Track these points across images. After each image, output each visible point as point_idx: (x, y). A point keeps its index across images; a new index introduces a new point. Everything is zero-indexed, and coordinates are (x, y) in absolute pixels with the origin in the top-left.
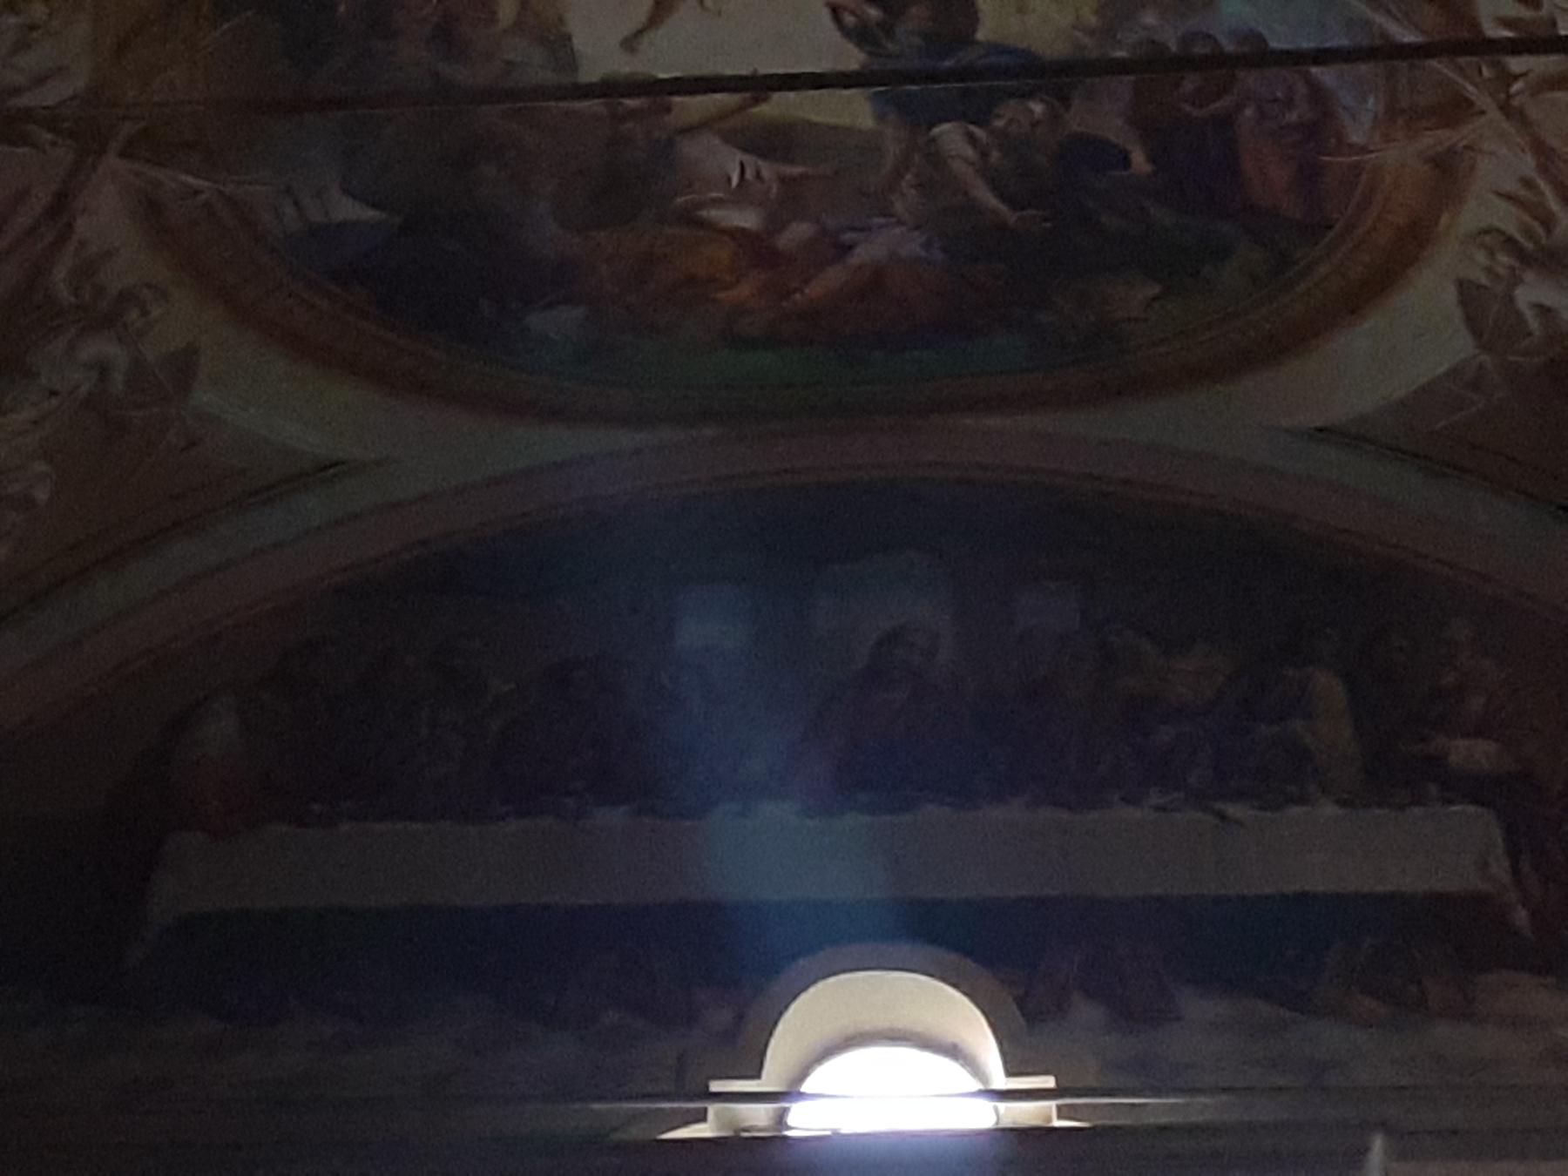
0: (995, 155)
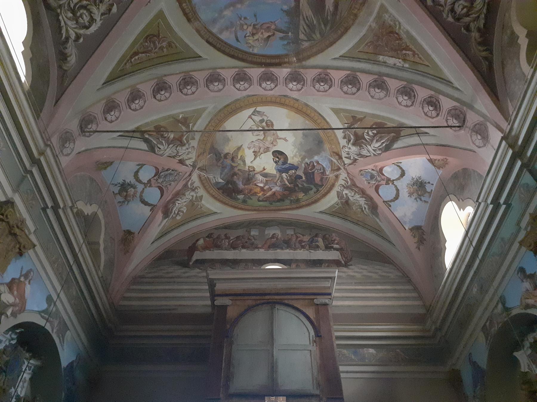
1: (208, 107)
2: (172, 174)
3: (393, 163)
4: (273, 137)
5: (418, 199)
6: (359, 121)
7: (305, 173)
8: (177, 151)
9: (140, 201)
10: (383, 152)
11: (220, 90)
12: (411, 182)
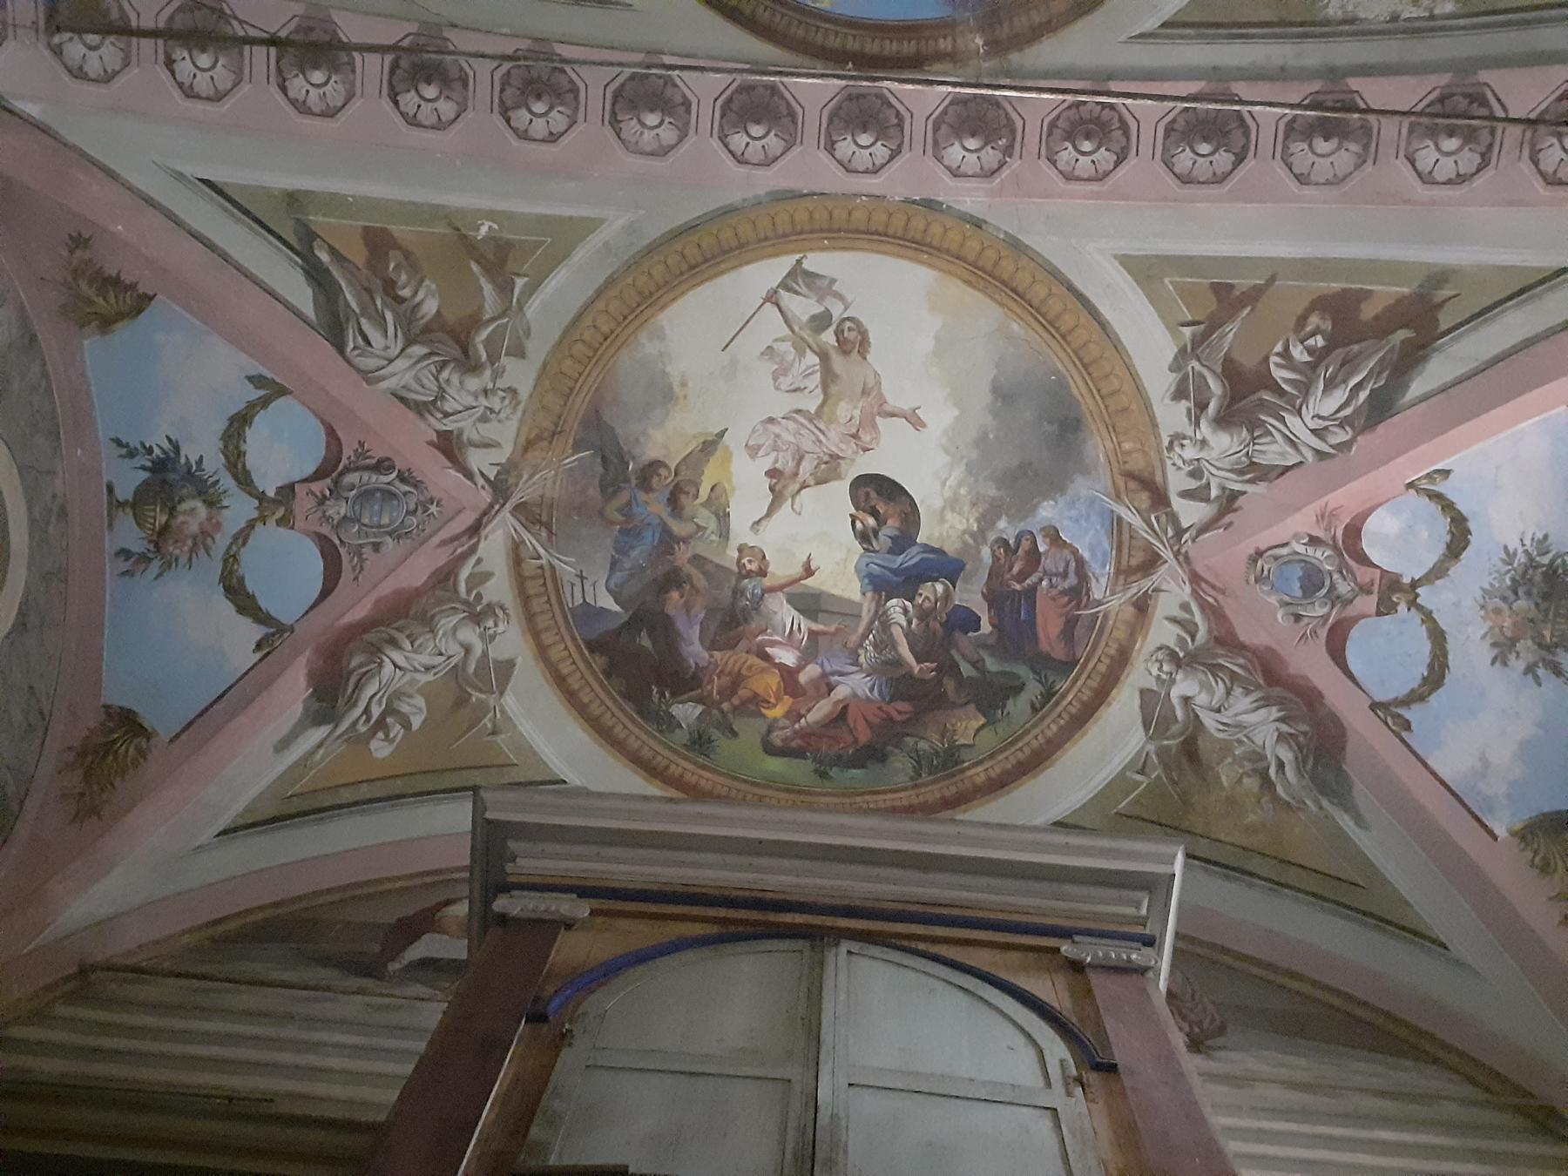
1: (602, 221)
2: (394, 495)
3: (1410, 485)
4: (860, 405)
5: (1541, 672)
6: (1244, 306)
7: (994, 598)
8: (440, 387)
9: (223, 579)
10: (1362, 431)
11: (663, 151)
12: (1502, 575)
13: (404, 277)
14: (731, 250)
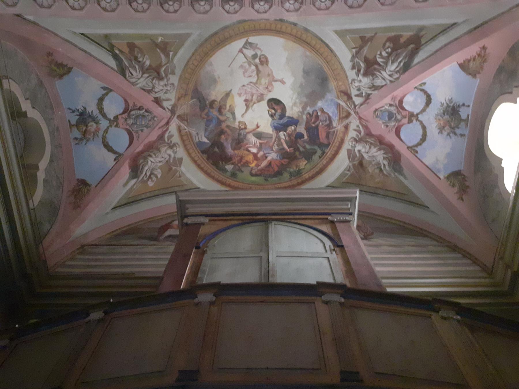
0: (287, 138)
3: (415, 88)
5: (451, 134)
7: (308, 129)
8: (153, 85)
11: (206, 12)
13: (139, 55)
14: (228, 38)
